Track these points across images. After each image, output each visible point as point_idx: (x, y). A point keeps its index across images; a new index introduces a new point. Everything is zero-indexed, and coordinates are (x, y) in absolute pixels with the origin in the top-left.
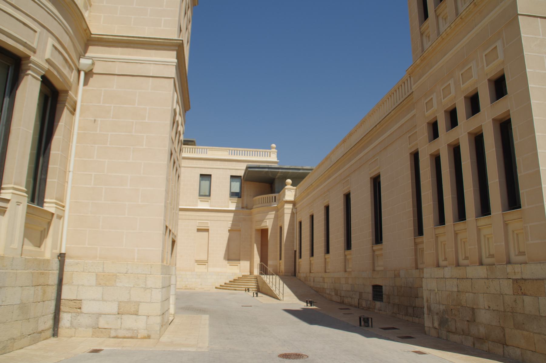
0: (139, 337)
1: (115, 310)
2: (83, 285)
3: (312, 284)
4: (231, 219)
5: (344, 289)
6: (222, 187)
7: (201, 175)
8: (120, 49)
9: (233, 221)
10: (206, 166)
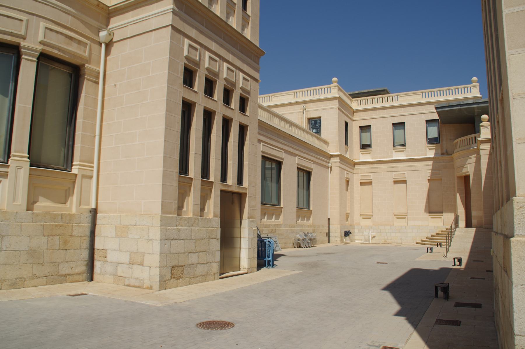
0: (144, 287)
1: (127, 261)
2: (107, 237)
4: (431, 167)
6: (417, 132)
7: (394, 124)
8: (131, 13)
9: (432, 170)
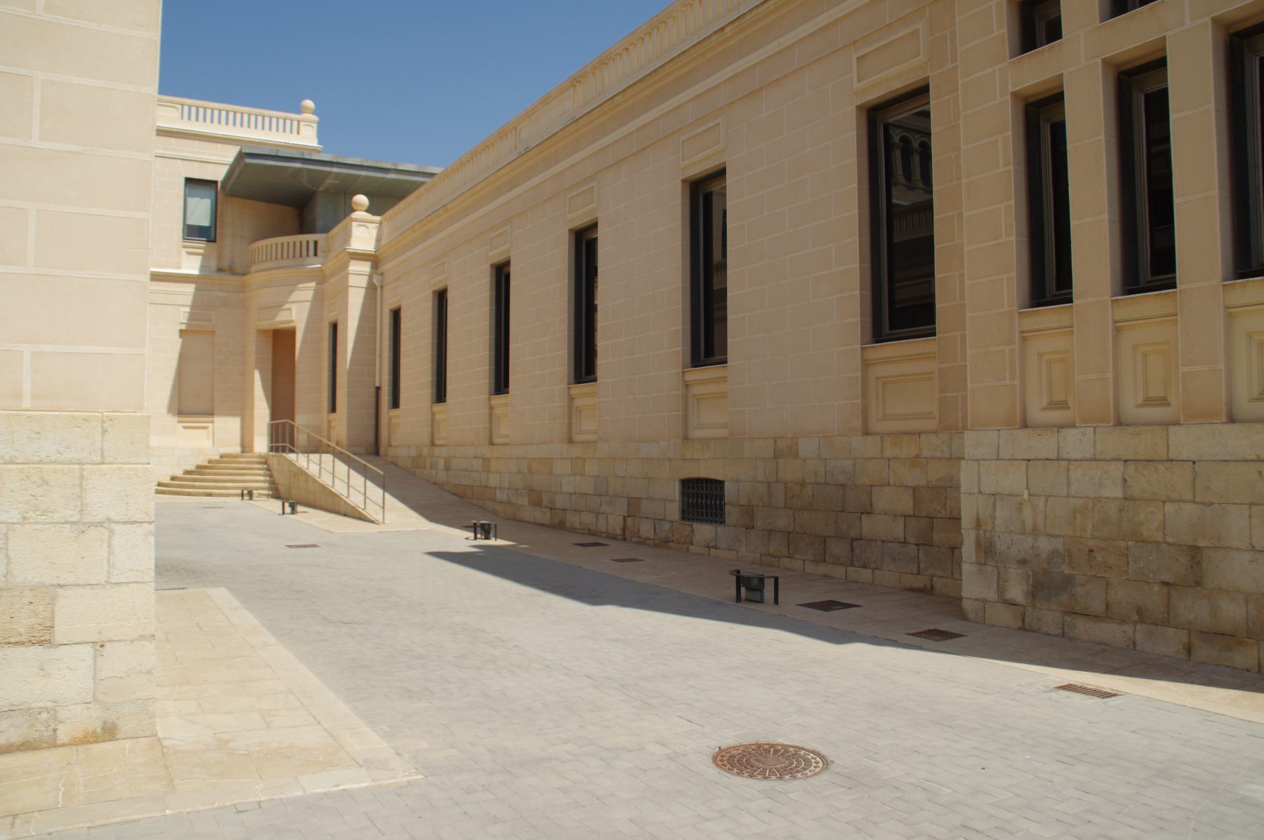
0: (62, 737)
3: (441, 476)
4: (189, 300)
5: (567, 488)
9: (192, 307)
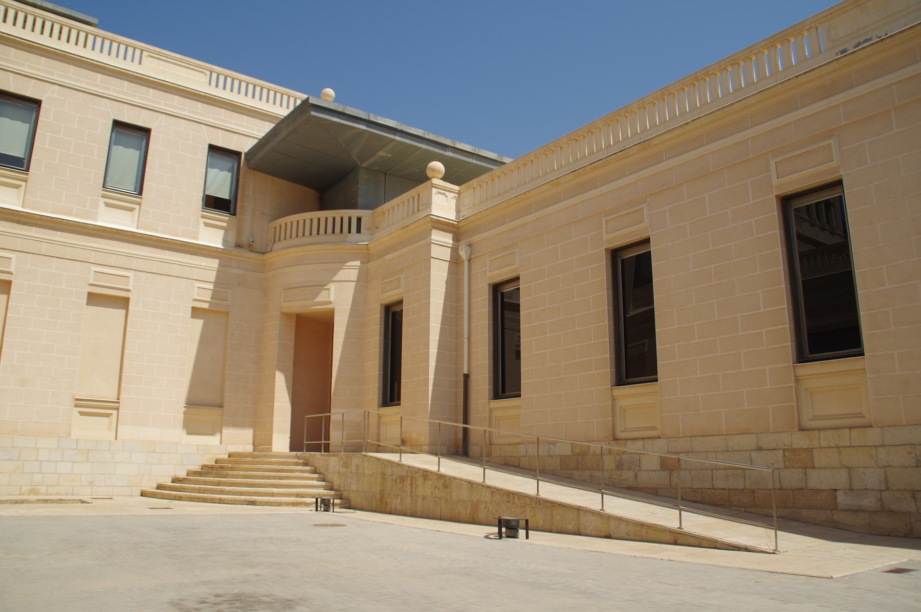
4: (212, 276)
6: (181, 174)
9: (216, 284)
10: (136, 100)
